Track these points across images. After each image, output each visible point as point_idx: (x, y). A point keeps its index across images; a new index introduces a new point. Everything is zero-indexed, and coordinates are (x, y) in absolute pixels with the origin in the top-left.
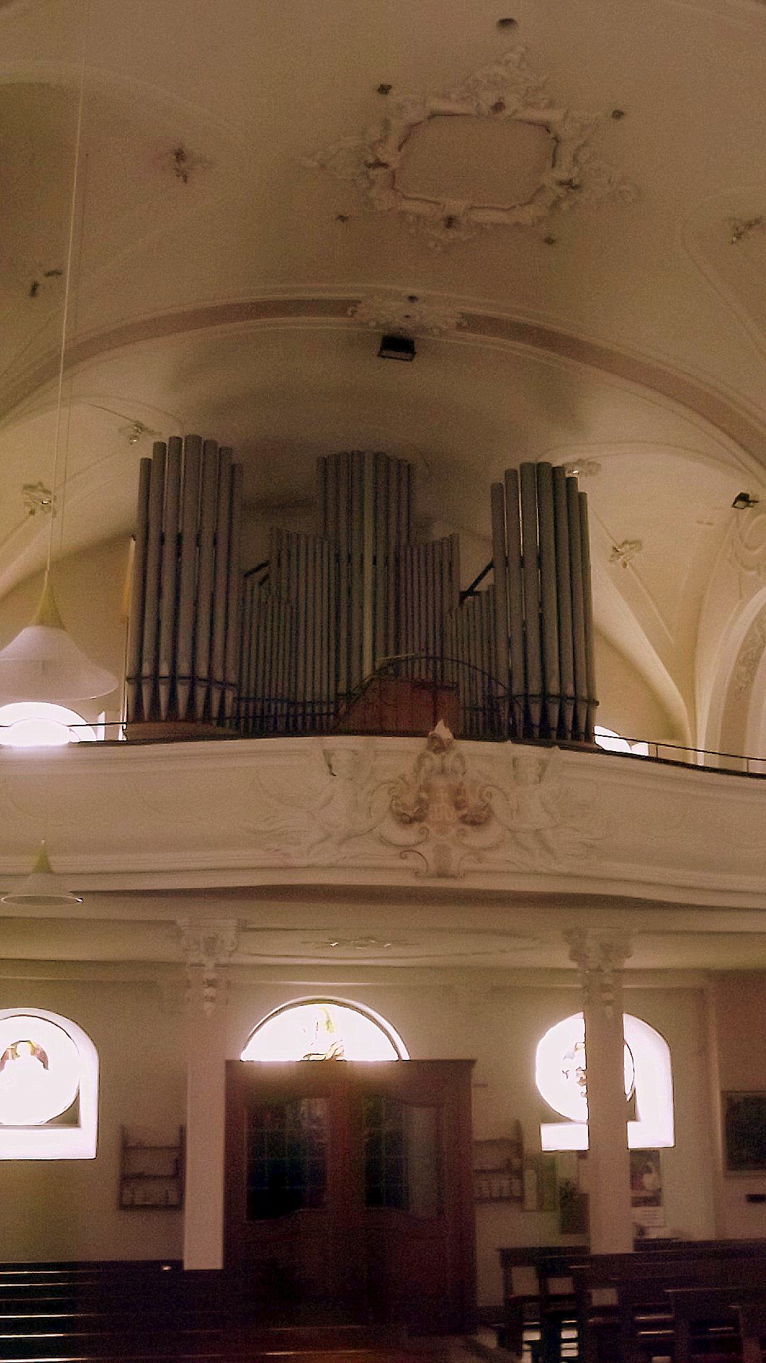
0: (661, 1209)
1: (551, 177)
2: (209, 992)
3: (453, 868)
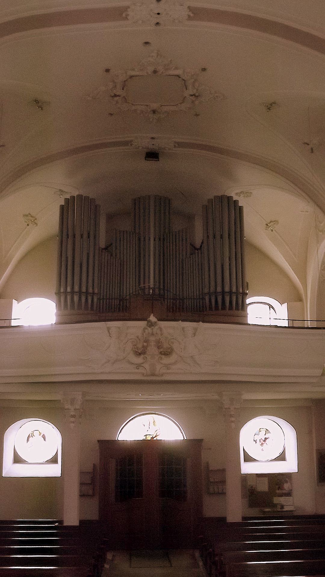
0: (292, 498)
1: (187, 93)
2: (72, 419)
3: (157, 372)
